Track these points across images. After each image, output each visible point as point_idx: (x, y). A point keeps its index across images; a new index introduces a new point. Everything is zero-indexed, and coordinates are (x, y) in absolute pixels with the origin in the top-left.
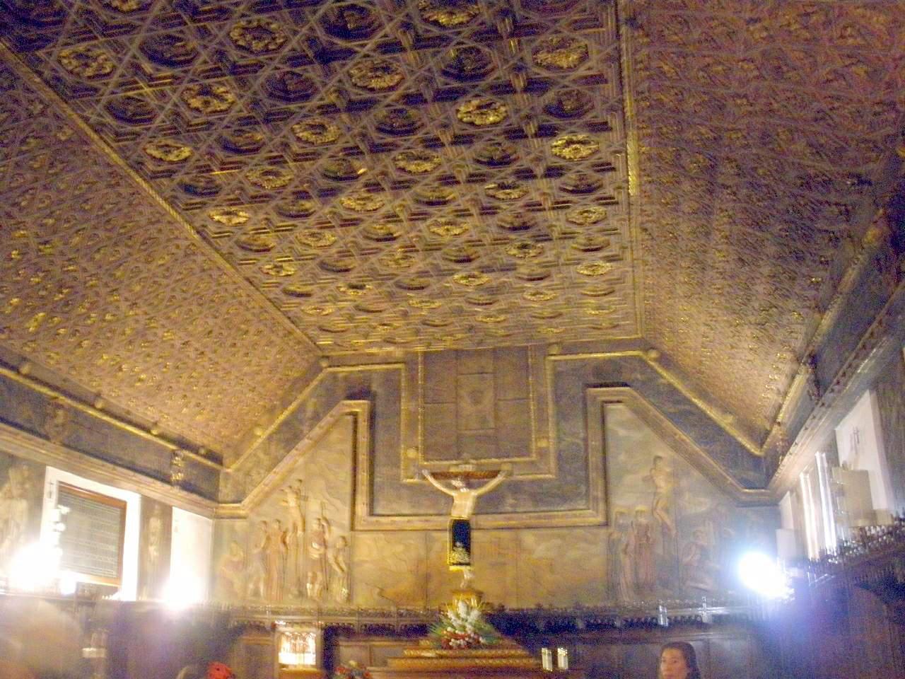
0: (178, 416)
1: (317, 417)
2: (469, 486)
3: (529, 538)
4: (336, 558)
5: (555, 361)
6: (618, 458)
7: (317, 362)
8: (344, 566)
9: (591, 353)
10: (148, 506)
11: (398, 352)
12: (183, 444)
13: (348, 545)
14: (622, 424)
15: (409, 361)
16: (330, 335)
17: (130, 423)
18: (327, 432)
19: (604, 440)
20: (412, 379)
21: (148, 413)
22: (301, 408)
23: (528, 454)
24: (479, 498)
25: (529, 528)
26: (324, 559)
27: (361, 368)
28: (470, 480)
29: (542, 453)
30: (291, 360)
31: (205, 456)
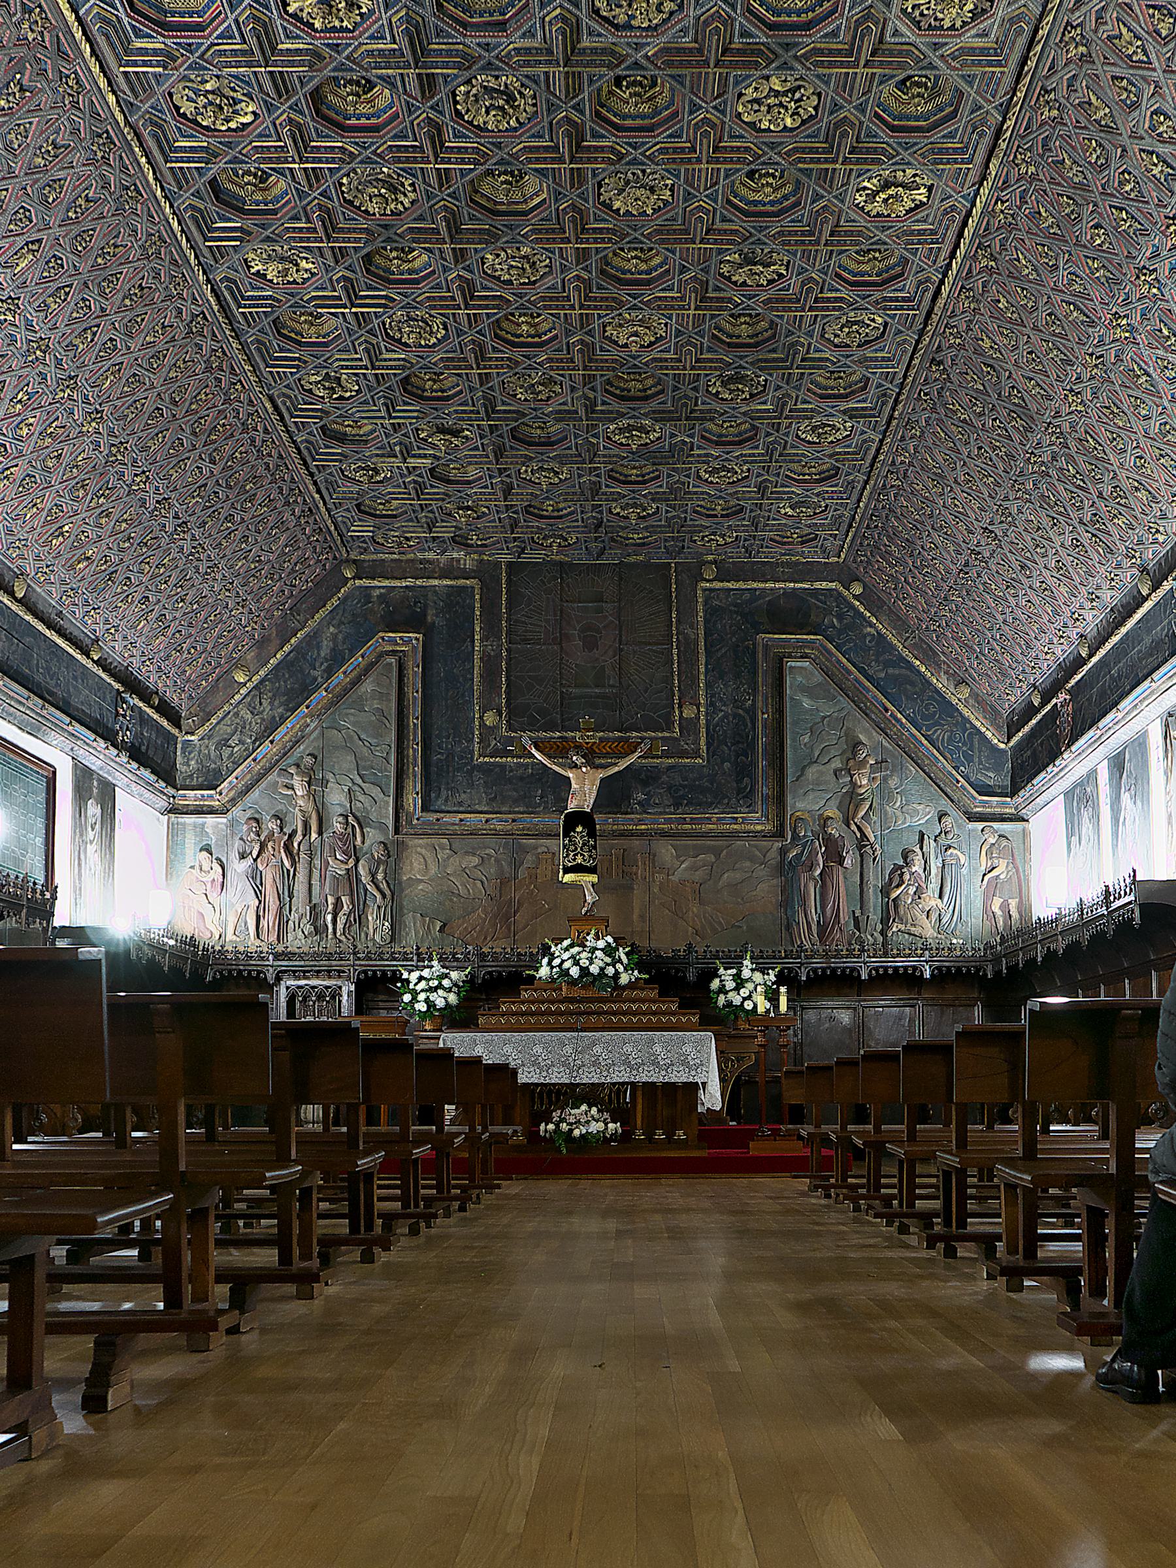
0: (130, 634)
1: (337, 660)
2: (590, 763)
3: (666, 851)
4: (373, 876)
5: (710, 590)
6: (796, 742)
7: (337, 569)
8: (384, 886)
9: (766, 582)
10: (83, 776)
11: (466, 559)
12: (133, 685)
13: (394, 853)
14: (804, 689)
15: (486, 573)
16: (371, 521)
17: (61, 632)
18: (356, 682)
19: (780, 712)
20: (490, 607)
21: (88, 624)
22: (313, 639)
23: (669, 727)
24: (602, 780)
25: (664, 834)
26: (352, 876)
27: (409, 582)
28: (592, 757)
29: (689, 727)
30: (303, 561)
31: (158, 709)
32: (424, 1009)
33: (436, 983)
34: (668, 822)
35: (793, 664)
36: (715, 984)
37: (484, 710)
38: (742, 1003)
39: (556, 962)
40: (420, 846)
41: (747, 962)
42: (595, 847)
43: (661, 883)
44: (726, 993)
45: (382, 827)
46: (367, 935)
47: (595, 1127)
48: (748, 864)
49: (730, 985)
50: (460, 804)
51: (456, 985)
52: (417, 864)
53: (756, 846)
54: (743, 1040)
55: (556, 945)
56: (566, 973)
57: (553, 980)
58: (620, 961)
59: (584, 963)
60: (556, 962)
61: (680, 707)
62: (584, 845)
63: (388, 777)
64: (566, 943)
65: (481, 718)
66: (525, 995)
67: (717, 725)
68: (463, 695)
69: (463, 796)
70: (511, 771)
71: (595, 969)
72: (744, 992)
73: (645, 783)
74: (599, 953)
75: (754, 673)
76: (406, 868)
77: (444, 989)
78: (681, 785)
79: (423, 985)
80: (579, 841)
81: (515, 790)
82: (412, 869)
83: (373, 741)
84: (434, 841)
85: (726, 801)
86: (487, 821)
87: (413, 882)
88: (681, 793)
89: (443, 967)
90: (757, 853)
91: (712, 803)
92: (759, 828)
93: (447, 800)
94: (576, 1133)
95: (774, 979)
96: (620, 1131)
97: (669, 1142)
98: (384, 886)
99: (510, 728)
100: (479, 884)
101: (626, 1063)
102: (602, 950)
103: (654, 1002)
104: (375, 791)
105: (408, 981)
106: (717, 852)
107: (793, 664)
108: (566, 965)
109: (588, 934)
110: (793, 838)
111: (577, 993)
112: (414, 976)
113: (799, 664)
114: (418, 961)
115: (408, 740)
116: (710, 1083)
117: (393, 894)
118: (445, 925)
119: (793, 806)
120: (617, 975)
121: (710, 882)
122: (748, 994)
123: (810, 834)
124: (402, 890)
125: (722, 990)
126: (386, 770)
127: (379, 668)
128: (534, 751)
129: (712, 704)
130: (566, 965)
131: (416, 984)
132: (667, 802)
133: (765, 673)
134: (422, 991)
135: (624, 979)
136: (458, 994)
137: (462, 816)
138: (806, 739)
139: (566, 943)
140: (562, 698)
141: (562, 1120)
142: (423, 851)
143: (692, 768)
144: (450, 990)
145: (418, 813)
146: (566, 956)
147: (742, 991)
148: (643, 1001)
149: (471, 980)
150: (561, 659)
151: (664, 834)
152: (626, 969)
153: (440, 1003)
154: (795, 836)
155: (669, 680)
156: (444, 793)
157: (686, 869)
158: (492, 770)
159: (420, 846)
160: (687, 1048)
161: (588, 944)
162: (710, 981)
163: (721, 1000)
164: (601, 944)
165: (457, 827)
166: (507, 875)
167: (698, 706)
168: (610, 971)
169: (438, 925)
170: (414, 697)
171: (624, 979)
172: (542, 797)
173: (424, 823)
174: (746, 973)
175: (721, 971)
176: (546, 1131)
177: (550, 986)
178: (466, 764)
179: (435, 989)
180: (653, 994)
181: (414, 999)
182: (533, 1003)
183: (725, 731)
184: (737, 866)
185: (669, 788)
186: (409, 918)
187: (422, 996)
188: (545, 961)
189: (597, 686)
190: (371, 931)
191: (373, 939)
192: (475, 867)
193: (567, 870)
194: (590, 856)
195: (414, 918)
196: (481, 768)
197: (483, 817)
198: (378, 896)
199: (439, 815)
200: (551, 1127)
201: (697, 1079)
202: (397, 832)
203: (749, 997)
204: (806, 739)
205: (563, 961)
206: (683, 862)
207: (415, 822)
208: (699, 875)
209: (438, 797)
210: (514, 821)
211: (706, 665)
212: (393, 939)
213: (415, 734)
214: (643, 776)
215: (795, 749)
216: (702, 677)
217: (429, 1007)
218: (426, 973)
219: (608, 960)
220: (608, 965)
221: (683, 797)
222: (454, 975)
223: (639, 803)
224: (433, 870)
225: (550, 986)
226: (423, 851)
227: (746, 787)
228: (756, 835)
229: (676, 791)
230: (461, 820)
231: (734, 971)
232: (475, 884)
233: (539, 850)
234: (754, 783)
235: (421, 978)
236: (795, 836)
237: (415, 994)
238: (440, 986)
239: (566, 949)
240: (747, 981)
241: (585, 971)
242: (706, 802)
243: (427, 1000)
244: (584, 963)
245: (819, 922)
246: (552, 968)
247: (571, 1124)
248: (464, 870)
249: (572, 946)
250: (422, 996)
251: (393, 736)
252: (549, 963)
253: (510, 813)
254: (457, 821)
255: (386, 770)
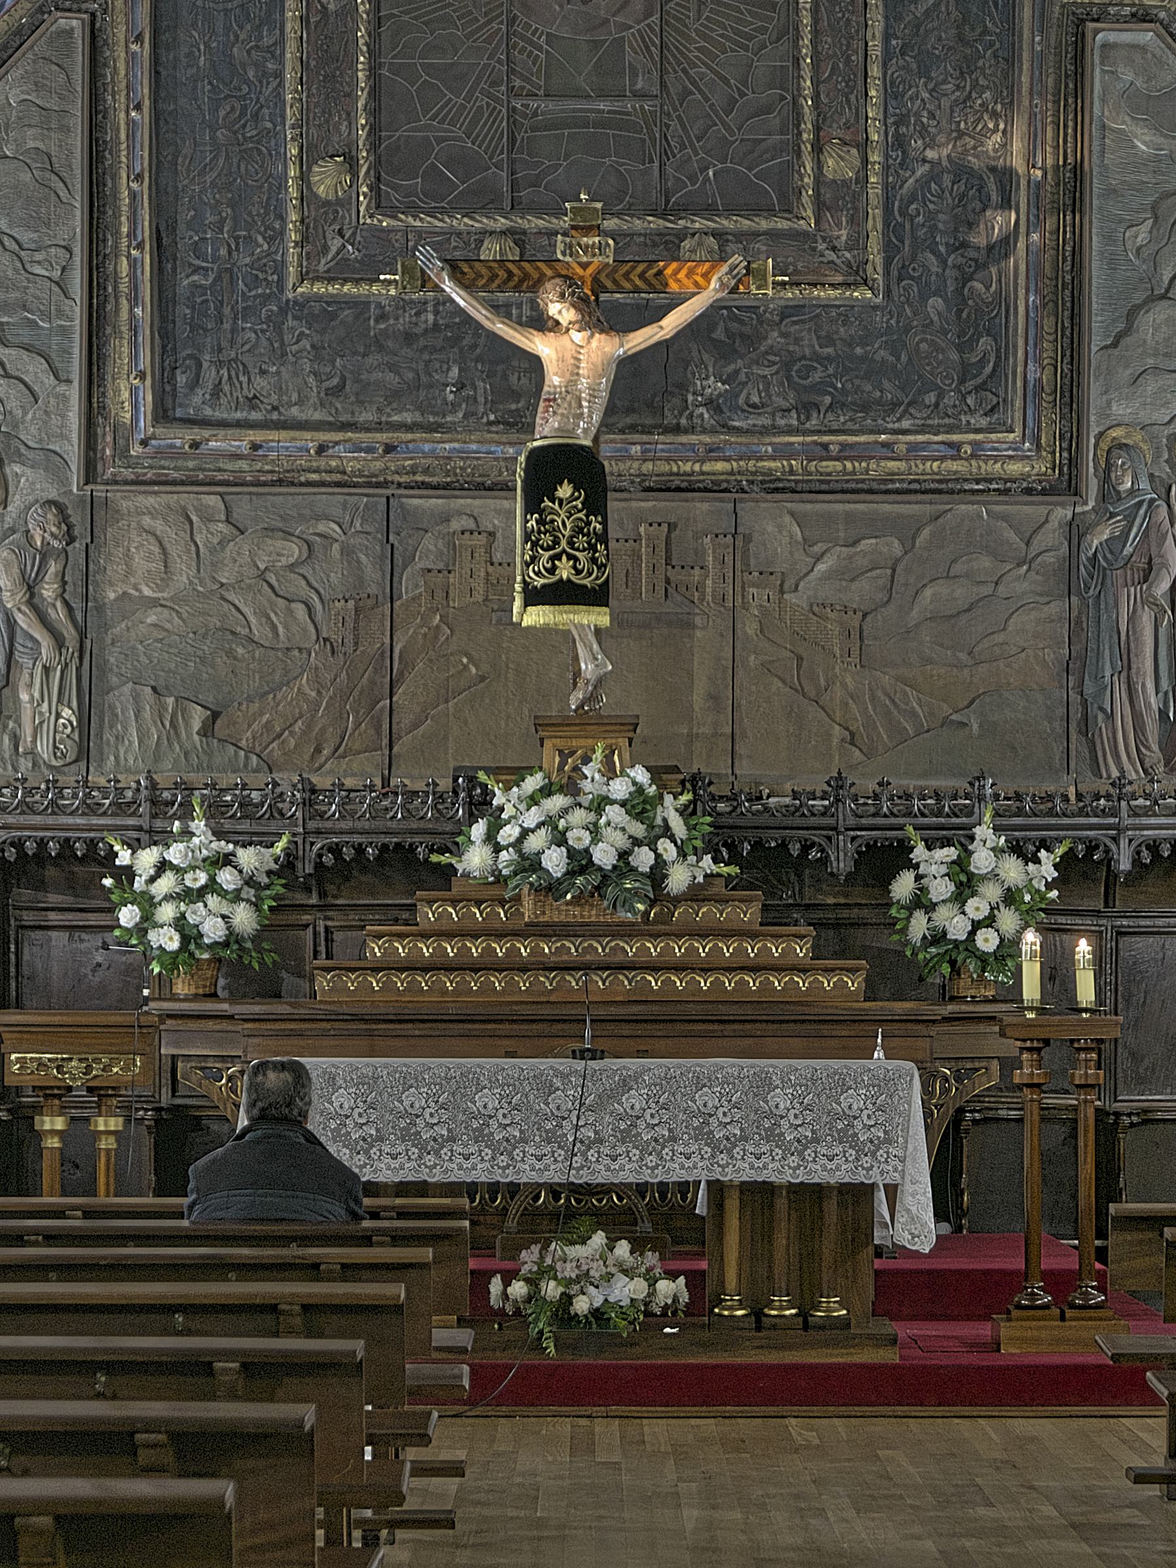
8: (59, 614)
25: (774, 487)
32: (174, 945)
33: (203, 878)
34: (783, 452)
35: (1112, 37)
36: (903, 886)
37: (307, 160)
38: (972, 933)
39: (509, 833)
40: (152, 513)
41: (983, 832)
42: (603, 538)
43: (765, 612)
44: (930, 908)
45: (52, 462)
46: (16, 740)
47: (626, 1290)
48: (986, 562)
49: (941, 889)
50: (252, 402)
51: (250, 882)
52: (143, 560)
53: (1004, 518)
54: (972, 1028)
55: (507, 789)
56: (530, 864)
57: (500, 880)
58: (667, 831)
59: (579, 838)
60: (509, 833)
61: (818, 149)
62: (578, 531)
63: (65, 332)
64: (532, 783)
65: (304, 177)
66: (429, 915)
67: (913, 198)
68: (256, 116)
69: (260, 383)
70: (382, 317)
71: (604, 856)
72: (977, 907)
73: (725, 352)
74: (614, 813)
75: (1011, 60)
76: (115, 569)
77: (222, 893)
78: (818, 358)
79: (166, 883)
80: (561, 519)
81: (393, 368)
82: (129, 572)
83: (26, 237)
84: (185, 498)
85: (930, 398)
86: (321, 449)
87: (130, 604)
88: (817, 376)
89: (219, 834)
90: (1010, 535)
91: (895, 405)
92: (1015, 468)
93: (217, 392)
94: (581, 1305)
95: (1050, 873)
96: (685, 1297)
97: (806, 1327)
98: (59, 614)
99: (379, 204)
100: (300, 611)
101: (703, 1134)
102: (623, 804)
103: (754, 936)
104: (34, 369)
105: (128, 873)
106: (908, 532)
107: (1112, 37)
108: (535, 842)
109: (587, 760)
110: (1103, 497)
111: (561, 911)
112: (147, 858)
113: (1126, 37)
114: (154, 816)
115: (117, 234)
116: (908, 1188)
117: (83, 635)
118: (215, 715)
119: (1104, 414)
120: (658, 873)
121: (891, 609)
122: (985, 911)
123: (1144, 484)
124: (105, 627)
125: (921, 902)
126: (60, 314)
127: (39, 44)
128: (448, 286)
129: (900, 143)
130: (535, 842)
131: (152, 880)
132: (779, 402)
133: (1039, 60)
134: (168, 898)
135: (678, 879)
136: (257, 906)
137: (257, 436)
138: (1142, 234)
139: (532, 783)
140: (513, 124)
141: (547, 1272)
142: (159, 526)
143: (847, 312)
144: (236, 897)
145: (144, 424)
146: (531, 818)
147: (971, 904)
148: (726, 934)
149: (287, 865)
150: (512, 21)
151: (774, 487)
152: (682, 854)
153: (213, 930)
154: (1108, 493)
155: (786, 79)
156: (210, 375)
157: (828, 576)
158: (333, 316)
159: (152, 513)
160: (853, 1100)
161: (586, 785)
162: (893, 876)
163: (919, 926)
164: (619, 788)
165: (243, 465)
166: (373, 589)
167: (864, 146)
168: (644, 859)
169: (198, 716)
170: (131, 124)
171: (678, 879)
172: (460, 386)
173: (159, 453)
174: (982, 860)
175: (919, 852)
176: (505, 1296)
177: (495, 892)
178: (266, 299)
179: (201, 893)
180: (749, 914)
181: (147, 921)
182: (449, 935)
183: (931, 216)
184: (958, 568)
185: (787, 366)
186: (121, 697)
187: (167, 912)
188: (478, 830)
189: (602, 95)
190: (28, 730)
191: (32, 753)
192: (291, 567)
193: (533, 597)
194: (594, 560)
195: (136, 697)
196: (302, 304)
197: (310, 440)
198: (46, 644)
199: (197, 433)
200: (518, 1289)
201: (875, 1177)
202: (90, 473)
203: (990, 921)
204: (1142, 234)
205: (525, 833)
206: (819, 558)
207: (136, 450)
208: (863, 591)
209: (194, 384)
210: (389, 449)
211: (887, 38)
212: (84, 753)
213: (133, 221)
214: (719, 334)
215: (1112, 263)
216: (875, 71)
217: (185, 940)
218: (175, 853)
219: (638, 829)
220: (637, 842)
221: (820, 388)
222: (248, 858)
223: (709, 403)
224: (184, 573)
225: (495, 892)
226: (159, 526)
227: (983, 361)
228: (1005, 489)
229: (808, 371)
230: (255, 447)
231: (951, 853)
232: (290, 612)
233: (456, 525)
234: (1003, 354)
235: (163, 866)
236: (1108, 493)
237: (148, 904)
238: (212, 886)
239: (533, 800)
240: (983, 878)
241: (580, 862)
242: (879, 402)
243: (180, 923)
244: (579, 838)
245: (1163, 713)
246: (497, 849)
247: (569, 1282)
248: (262, 575)
249: (546, 791)
250: (167, 912)
251: (77, 222)
252: (490, 838)
253: (379, 427)
254: (244, 446)
255: (60, 314)
